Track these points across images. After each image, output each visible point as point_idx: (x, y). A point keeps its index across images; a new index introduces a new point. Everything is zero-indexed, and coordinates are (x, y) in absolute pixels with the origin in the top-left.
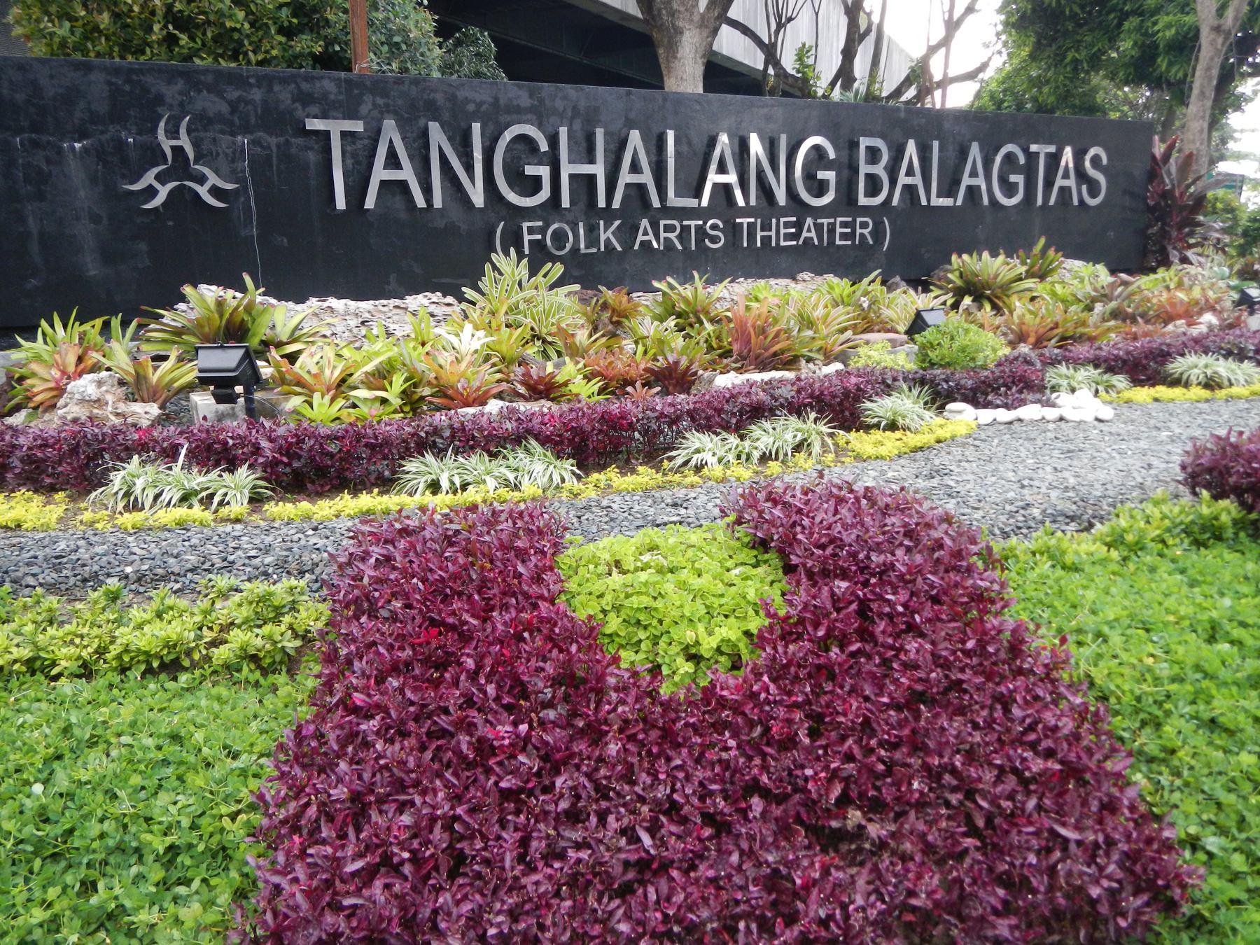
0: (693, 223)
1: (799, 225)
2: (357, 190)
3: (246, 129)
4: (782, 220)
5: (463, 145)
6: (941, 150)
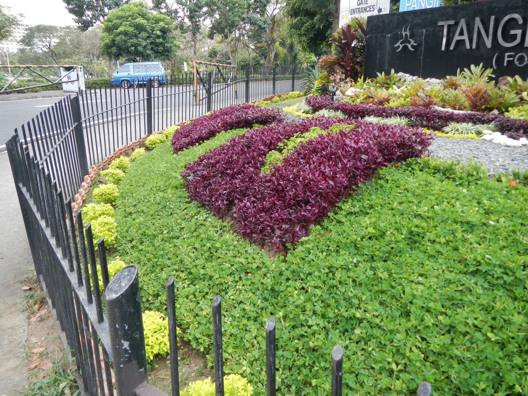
2: (448, 44)
3: (425, 27)
5: (485, 23)
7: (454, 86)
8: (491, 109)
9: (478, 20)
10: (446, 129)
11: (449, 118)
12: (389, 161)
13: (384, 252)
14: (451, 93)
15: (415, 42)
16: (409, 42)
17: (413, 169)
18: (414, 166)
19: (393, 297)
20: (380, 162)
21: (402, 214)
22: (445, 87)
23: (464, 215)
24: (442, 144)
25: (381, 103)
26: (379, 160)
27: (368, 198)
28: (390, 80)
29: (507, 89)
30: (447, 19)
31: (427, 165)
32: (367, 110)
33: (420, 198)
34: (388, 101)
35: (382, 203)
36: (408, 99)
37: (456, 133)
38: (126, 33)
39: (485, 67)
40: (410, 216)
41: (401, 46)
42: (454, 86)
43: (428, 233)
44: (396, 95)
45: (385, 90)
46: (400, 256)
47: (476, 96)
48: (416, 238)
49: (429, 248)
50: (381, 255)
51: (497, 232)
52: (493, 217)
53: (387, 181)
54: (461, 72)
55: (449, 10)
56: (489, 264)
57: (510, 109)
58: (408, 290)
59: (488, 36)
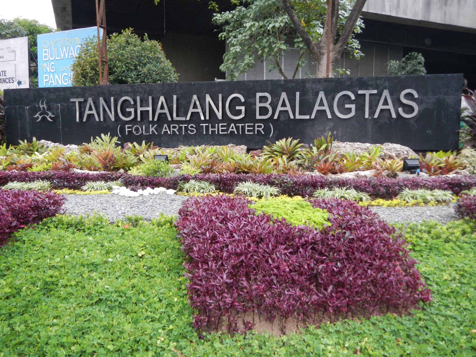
0: (183, 126)
1: (228, 126)
2: (81, 117)
3: (60, 102)
4: (220, 125)
5: (107, 102)
6: (300, 97)
7: (89, 151)
8: (118, 169)
9: (101, 99)
10: (84, 188)
11: (87, 178)
12: (26, 223)
13: (20, 307)
14: (87, 157)
15: (53, 114)
16: (48, 114)
17: (49, 227)
18: (49, 225)
19: (30, 344)
20: (15, 226)
21: (38, 269)
22: (82, 152)
23: (89, 258)
24: (80, 201)
25: (24, 168)
26: (14, 224)
27: (4, 261)
28: (33, 147)
29: (129, 152)
30: (77, 97)
31: (61, 222)
32: (10, 176)
33: (54, 252)
34: (31, 166)
35: (19, 263)
36: (51, 164)
37: (92, 190)
39: (112, 136)
40: (45, 269)
41: (40, 117)
42: (89, 151)
43: (61, 280)
44: (39, 160)
45: (28, 156)
46: (37, 307)
47: (105, 159)
48: (52, 287)
49: (62, 293)
50: (18, 310)
51: (114, 266)
52: (111, 255)
53: (24, 242)
54: (94, 139)
55: (78, 90)
56: (108, 292)
57: (131, 168)
58: (43, 334)
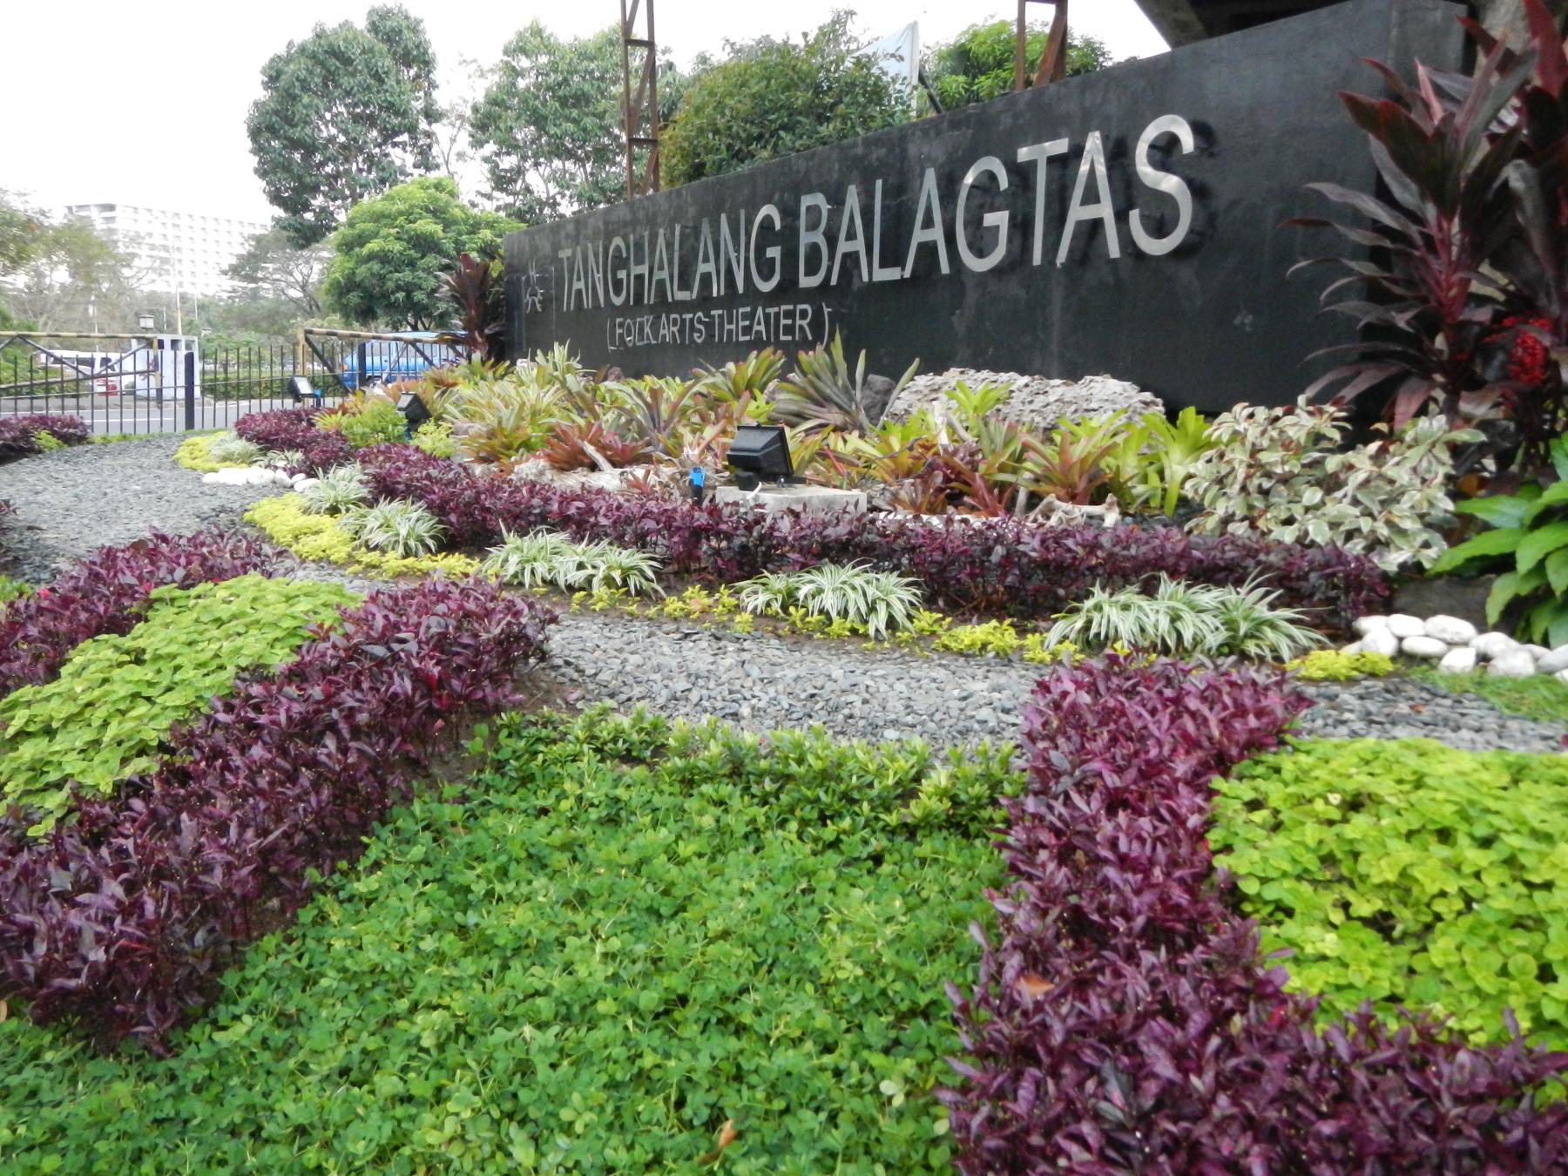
0: (688, 316)
2: (1051, 248)
38: (383, 258)
59: (1092, 171)
